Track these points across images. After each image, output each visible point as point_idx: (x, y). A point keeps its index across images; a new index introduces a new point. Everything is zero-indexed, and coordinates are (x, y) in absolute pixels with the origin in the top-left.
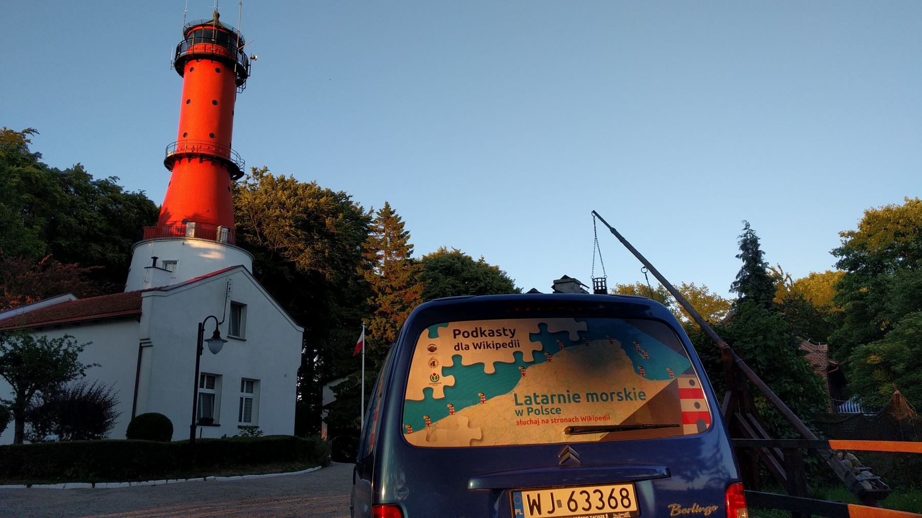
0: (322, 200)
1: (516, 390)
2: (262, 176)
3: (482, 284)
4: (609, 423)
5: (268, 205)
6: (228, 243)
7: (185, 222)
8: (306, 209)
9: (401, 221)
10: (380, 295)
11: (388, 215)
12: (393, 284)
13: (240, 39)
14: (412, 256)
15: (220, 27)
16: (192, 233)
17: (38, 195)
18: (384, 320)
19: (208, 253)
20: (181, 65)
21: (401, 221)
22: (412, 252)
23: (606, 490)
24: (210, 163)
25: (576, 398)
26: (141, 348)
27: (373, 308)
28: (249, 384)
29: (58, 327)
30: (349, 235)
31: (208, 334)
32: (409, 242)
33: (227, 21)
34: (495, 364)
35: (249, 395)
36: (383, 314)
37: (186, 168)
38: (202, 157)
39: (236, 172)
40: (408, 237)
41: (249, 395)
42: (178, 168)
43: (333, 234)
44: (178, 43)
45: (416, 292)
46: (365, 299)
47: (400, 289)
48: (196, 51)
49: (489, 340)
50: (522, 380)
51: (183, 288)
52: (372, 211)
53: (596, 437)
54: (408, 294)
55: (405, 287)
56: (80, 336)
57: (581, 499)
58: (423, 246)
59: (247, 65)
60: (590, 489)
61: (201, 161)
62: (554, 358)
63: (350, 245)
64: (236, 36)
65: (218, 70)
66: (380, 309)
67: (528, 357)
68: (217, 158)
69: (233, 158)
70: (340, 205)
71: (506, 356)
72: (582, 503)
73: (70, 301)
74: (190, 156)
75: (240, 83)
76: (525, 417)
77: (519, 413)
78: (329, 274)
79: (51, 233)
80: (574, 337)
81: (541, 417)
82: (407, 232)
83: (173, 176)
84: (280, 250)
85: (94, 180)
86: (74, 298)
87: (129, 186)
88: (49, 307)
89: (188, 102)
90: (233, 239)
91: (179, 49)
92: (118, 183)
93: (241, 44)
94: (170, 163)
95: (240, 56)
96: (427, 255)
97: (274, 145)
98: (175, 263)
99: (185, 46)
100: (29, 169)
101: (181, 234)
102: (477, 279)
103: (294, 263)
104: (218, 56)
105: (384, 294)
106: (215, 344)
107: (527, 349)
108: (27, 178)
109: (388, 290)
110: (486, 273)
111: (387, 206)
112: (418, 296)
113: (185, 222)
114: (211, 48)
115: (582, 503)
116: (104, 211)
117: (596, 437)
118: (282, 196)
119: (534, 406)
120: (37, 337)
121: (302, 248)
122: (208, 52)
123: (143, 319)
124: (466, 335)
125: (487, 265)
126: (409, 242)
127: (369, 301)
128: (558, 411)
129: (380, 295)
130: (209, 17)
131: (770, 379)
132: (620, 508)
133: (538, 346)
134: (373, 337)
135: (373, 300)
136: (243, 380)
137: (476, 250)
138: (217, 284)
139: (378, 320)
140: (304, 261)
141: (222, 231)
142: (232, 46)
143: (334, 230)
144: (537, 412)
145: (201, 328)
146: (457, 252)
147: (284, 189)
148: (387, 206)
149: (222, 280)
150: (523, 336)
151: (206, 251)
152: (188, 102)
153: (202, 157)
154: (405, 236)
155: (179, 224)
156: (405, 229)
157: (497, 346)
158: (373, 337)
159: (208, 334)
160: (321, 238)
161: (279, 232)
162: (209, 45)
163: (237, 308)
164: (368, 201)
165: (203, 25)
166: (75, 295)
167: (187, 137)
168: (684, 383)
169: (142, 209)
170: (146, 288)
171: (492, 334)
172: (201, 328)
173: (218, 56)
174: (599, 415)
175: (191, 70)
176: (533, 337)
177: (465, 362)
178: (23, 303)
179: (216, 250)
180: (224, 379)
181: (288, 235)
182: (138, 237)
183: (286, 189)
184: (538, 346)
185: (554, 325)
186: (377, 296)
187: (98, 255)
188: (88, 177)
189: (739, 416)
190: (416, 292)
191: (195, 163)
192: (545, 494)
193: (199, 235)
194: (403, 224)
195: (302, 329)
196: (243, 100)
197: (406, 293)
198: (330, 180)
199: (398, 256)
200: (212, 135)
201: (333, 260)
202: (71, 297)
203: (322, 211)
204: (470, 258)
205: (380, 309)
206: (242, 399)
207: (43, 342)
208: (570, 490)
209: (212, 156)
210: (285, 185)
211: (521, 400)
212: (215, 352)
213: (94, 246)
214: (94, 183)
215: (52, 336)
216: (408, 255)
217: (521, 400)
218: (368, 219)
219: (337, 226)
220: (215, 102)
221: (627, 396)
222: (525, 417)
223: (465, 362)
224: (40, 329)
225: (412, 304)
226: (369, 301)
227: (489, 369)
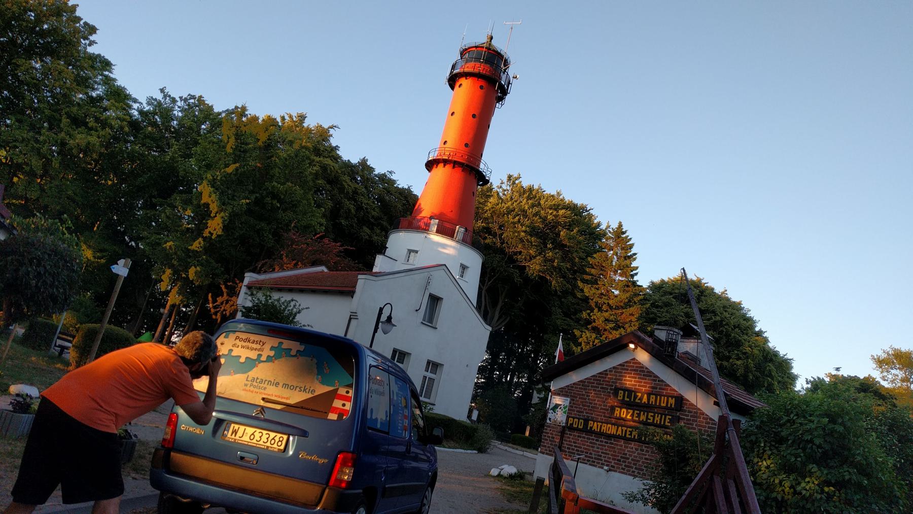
0: (561, 212)
1: (250, 373)
2: (514, 183)
3: (718, 318)
4: (288, 402)
5: (510, 211)
6: (464, 241)
7: (431, 218)
8: (544, 219)
9: (631, 242)
10: (596, 310)
11: (619, 232)
12: (611, 302)
13: (506, 61)
14: (635, 278)
15: (489, 49)
16: (435, 229)
17: (329, 182)
18: (594, 336)
19: (445, 249)
20: (453, 81)
21: (631, 242)
22: (636, 274)
23: (272, 435)
24: (461, 169)
25: (277, 384)
26: (350, 319)
27: (588, 322)
28: (433, 366)
29: (291, 290)
30: (581, 248)
31: (384, 318)
32: (634, 264)
33: (497, 44)
34: (247, 358)
35: (432, 376)
36: (596, 330)
37: (440, 171)
38: (455, 164)
39: (482, 179)
40: (635, 259)
41: (432, 376)
42: (434, 170)
43: (566, 246)
44: (454, 62)
45: (632, 315)
46: (581, 311)
47: (617, 308)
48: (466, 70)
49: (250, 345)
50: (255, 369)
51: (391, 276)
52: (608, 227)
53: (279, 407)
54: (624, 315)
55: (622, 308)
56: (303, 301)
57: (257, 435)
58: (650, 271)
59: (509, 83)
60: (265, 432)
61: (454, 167)
62: (276, 362)
63: (580, 258)
64: (502, 57)
65: (481, 87)
66: (594, 324)
67: (263, 358)
68: (467, 166)
69: (482, 167)
70: (578, 216)
71: (253, 355)
72: (257, 437)
73: (322, 272)
74: (445, 162)
75: (500, 99)
76: (248, 388)
77: (246, 385)
78: (555, 283)
79: (334, 214)
80: (293, 353)
81: (255, 390)
82: (635, 254)
83: (430, 178)
84: (516, 253)
85: (376, 173)
86: (326, 270)
87: (402, 183)
88: (296, 276)
89: (453, 114)
90: (469, 240)
91: (453, 67)
92: (393, 177)
93: (506, 63)
94: (430, 165)
95: (504, 77)
96: (666, 279)
97: (523, 156)
98: (417, 252)
99: (459, 66)
100: (328, 161)
101: (426, 229)
102: (714, 312)
103: (525, 267)
104: (486, 75)
105: (600, 309)
106: (387, 326)
107: (267, 352)
108: (324, 168)
109: (604, 307)
110: (724, 307)
111: (620, 225)
112: (634, 319)
113: (431, 218)
114: (480, 68)
115: (257, 437)
116: (380, 199)
117: (279, 407)
118: (525, 204)
119: (254, 383)
120: (276, 296)
121: (533, 254)
122: (476, 71)
123: (356, 296)
124: (241, 340)
125: (728, 299)
126: (634, 264)
127: (584, 315)
128: (265, 388)
129: (596, 310)
130: (482, 40)
131: (831, 464)
132: (275, 446)
133: (272, 353)
134: (582, 349)
135: (589, 314)
136: (429, 362)
137: (717, 282)
138: (420, 277)
139: (588, 335)
140: (534, 267)
141: (460, 230)
142: (498, 66)
143: (566, 242)
144: (255, 387)
145: (381, 310)
146: (700, 280)
147: (529, 198)
148: (620, 225)
149: (425, 274)
150: (267, 347)
151: (444, 246)
152: (453, 114)
153: (455, 164)
154: (632, 257)
155: (425, 220)
156: (633, 251)
157: (252, 349)
158: (582, 349)
159: (384, 318)
160: (554, 248)
161: (515, 236)
162: (478, 64)
163: (435, 300)
164: (605, 217)
165: (476, 47)
166: (327, 267)
167: (446, 145)
168: (342, 391)
169: (408, 201)
170: (396, 269)
171: (253, 342)
172: (381, 310)
173: (486, 75)
174: (284, 396)
175: (460, 86)
176: (272, 348)
177: (233, 354)
178: (295, 267)
179: (451, 246)
180: (412, 357)
181: (522, 240)
182: (395, 225)
183: (531, 199)
184: (272, 353)
185: (287, 344)
186: (592, 311)
187: (367, 237)
188: (371, 169)
189: (718, 481)
190: (632, 315)
191: (448, 168)
192: (242, 428)
193: (440, 231)
194: (631, 246)
195: (490, 329)
196: (501, 115)
197: (622, 313)
198: (573, 195)
199: (621, 275)
200: (466, 145)
201: (560, 269)
202: (323, 268)
203: (558, 223)
204: (713, 289)
205: (594, 324)
206: (425, 377)
207: (278, 300)
208: (254, 430)
209: (466, 165)
210: (531, 193)
211: (250, 379)
212: (385, 333)
213: (365, 228)
214: (376, 175)
215: (286, 297)
216: (632, 276)
217: (250, 379)
218: (604, 234)
219: (569, 239)
220: (474, 116)
221: (305, 390)
222: (248, 388)
223: (233, 354)
224: (280, 290)
225: (627, 326)
226: (584, 315)
227: (242, 360)
